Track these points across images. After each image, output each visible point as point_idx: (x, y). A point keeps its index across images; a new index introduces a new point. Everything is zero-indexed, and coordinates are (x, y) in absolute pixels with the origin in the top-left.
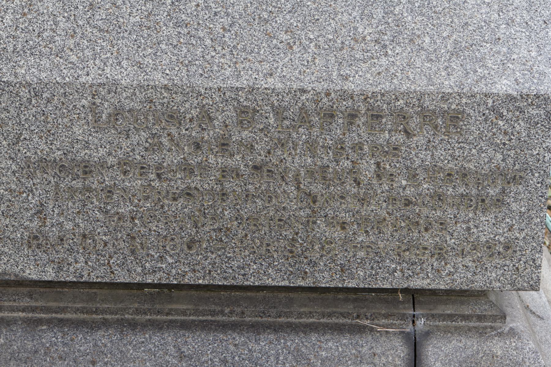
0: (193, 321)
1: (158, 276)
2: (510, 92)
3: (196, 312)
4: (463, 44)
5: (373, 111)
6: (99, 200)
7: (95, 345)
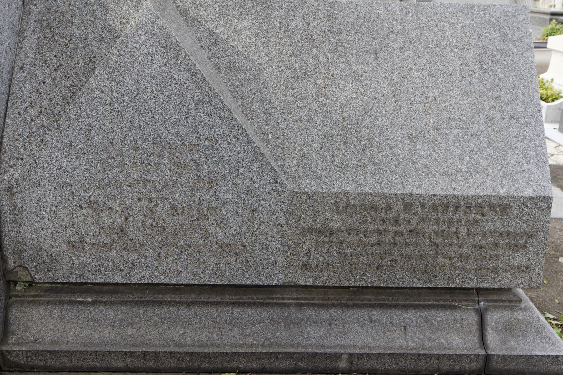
0: (375, 304)
1: (362, 282)
2: (531, 195)
3: (376, 300)
4: (508, 173)
5: (467, 204)
6: (336, 247)
7: (330, 316)
